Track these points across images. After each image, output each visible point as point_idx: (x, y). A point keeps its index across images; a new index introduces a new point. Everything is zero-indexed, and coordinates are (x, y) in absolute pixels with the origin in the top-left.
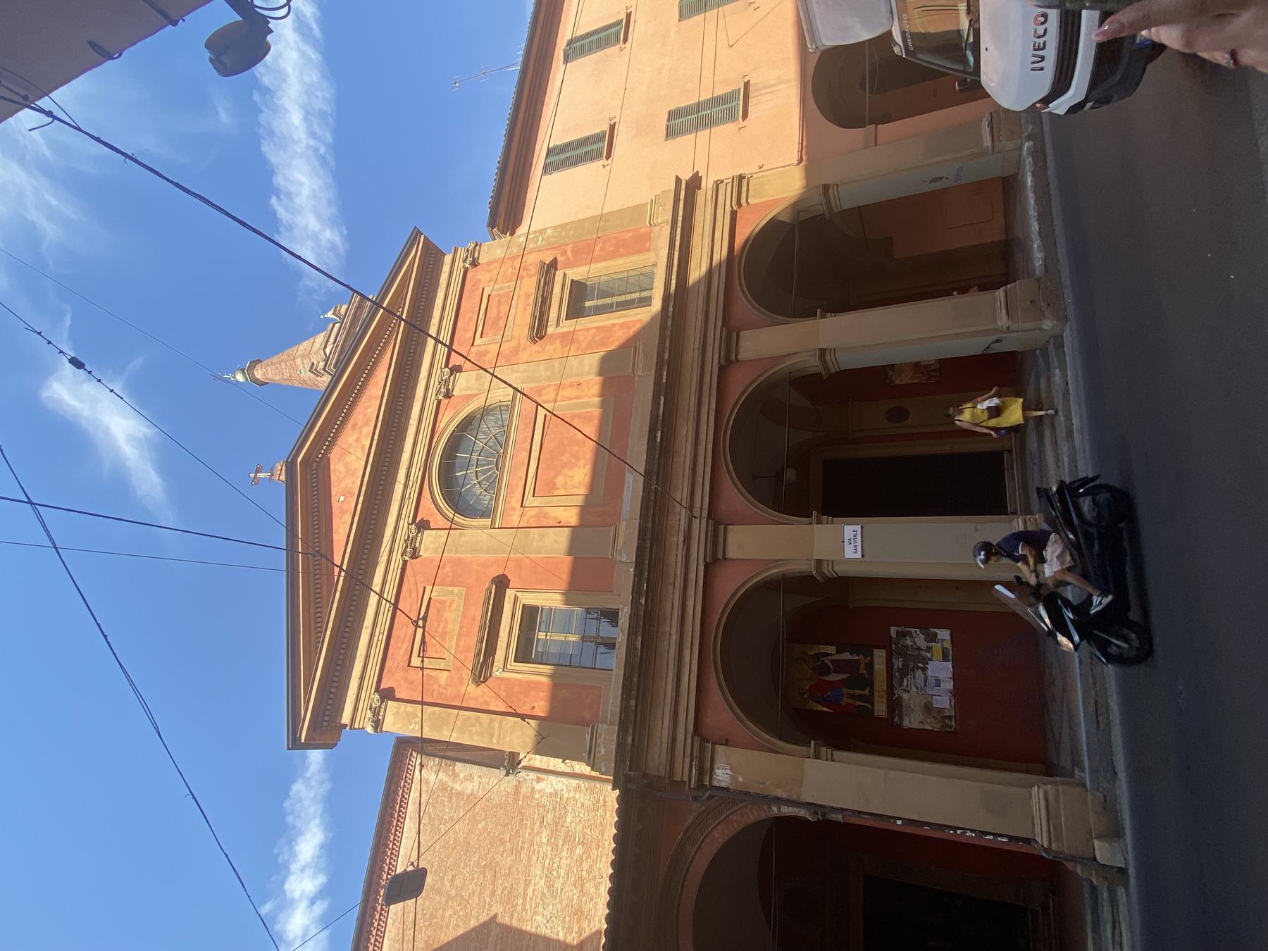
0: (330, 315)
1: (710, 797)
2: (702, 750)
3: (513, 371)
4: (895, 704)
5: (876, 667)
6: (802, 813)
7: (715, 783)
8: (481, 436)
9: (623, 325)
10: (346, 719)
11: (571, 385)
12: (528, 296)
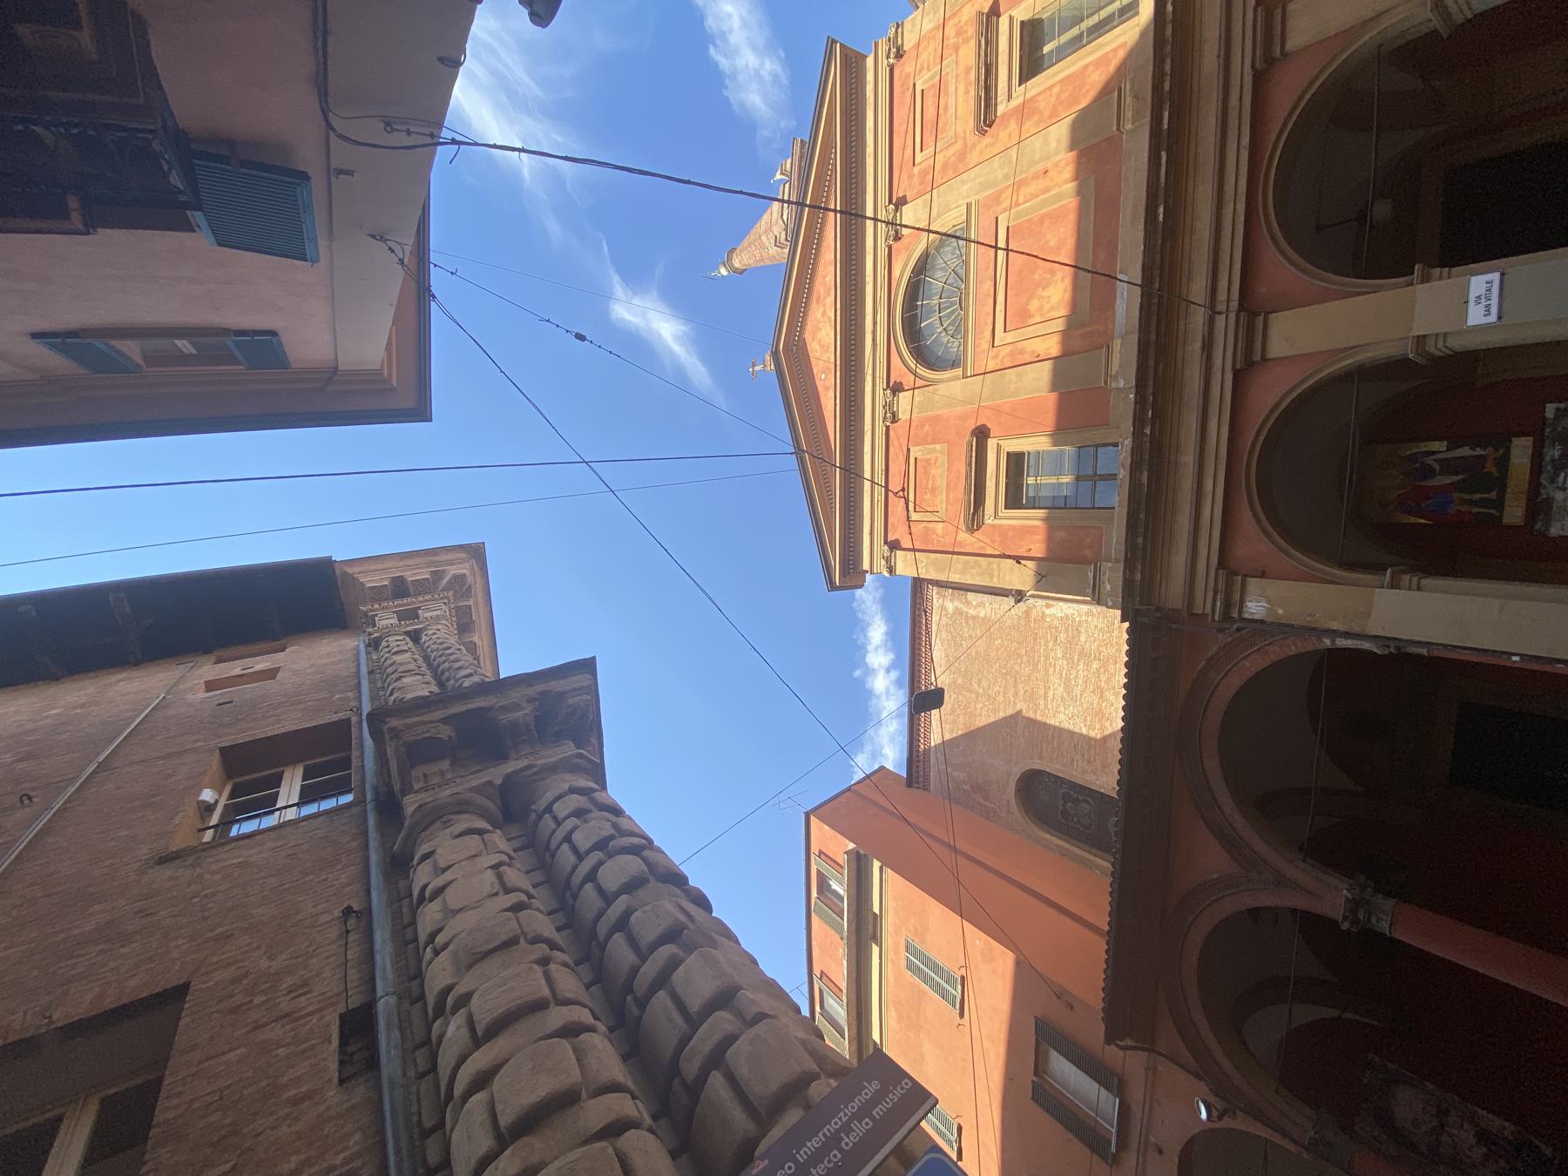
0: (778, 176)
1: (1238, 630)
2: (1229, 585)
3: (963, 183)
4: (1538, 506)
5: (1514, 460)
6: (1366, 645)
7: (1246, 616)
8: (939, 274)
9: (1098, 63)
10: (866, 566)
11: (1036, 177)
12: (968, 72)
